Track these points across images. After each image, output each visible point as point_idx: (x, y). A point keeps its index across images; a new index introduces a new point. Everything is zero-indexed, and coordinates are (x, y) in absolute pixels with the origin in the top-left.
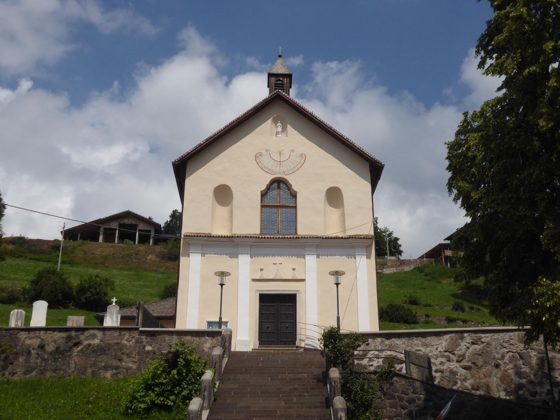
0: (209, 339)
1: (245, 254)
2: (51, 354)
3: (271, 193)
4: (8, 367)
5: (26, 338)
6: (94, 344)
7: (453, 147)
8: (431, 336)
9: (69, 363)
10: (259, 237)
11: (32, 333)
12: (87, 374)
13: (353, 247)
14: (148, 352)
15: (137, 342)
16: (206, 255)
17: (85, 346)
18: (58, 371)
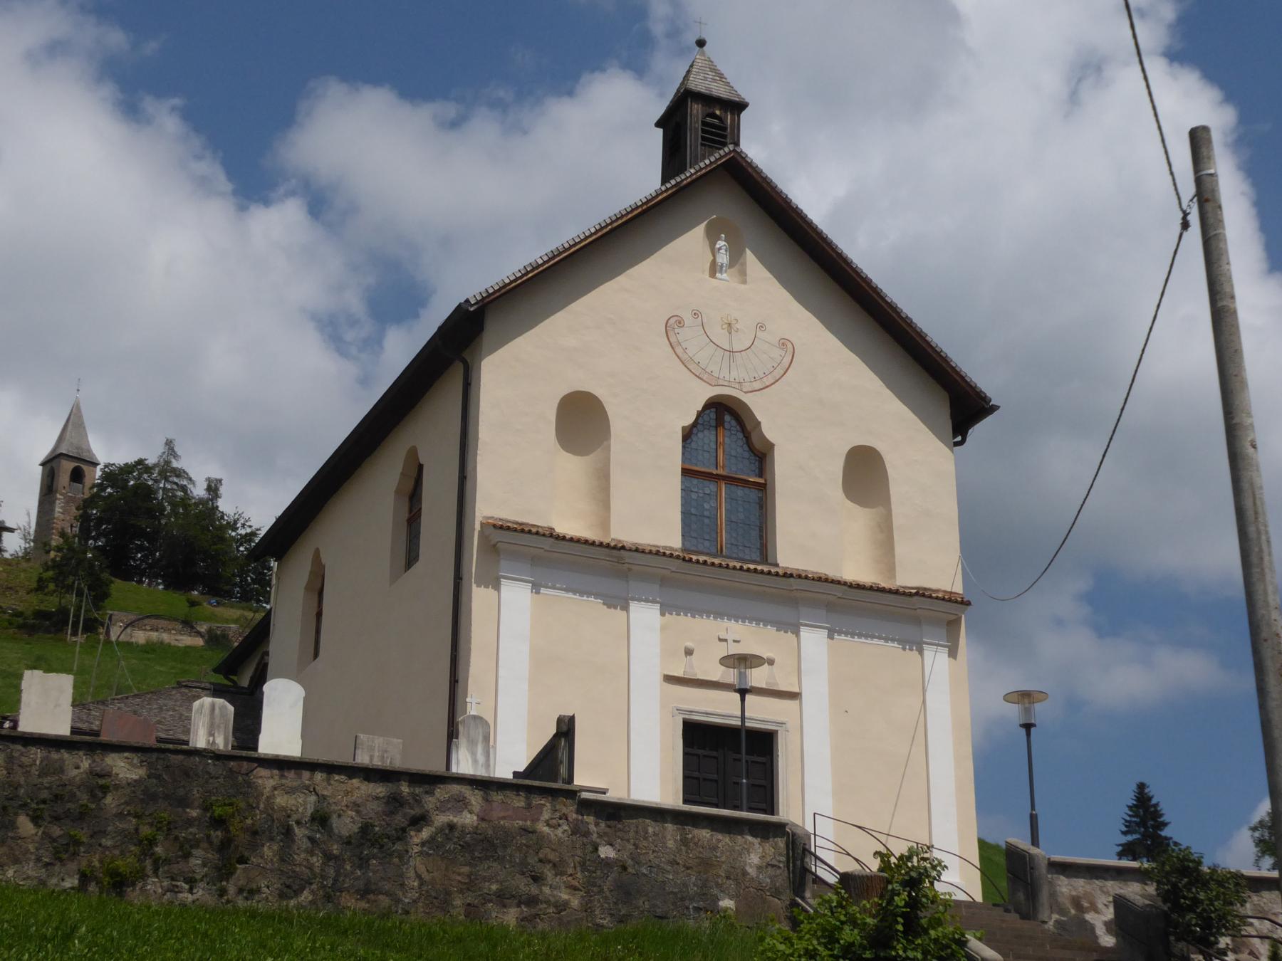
0: (756, 841)
1: (647, 601)
2: (349, 843)
3: (700, 435)
4: (236, 869)
5: (275, 788)
6: (463, 826)
7: (460, 305)
8: (1270, 889)
9: (402, 876)
10: (678, 557)
11: (291, 774)
12: (454, 912)
13: (917, 621)
14: (607, 863)
15: (575, 832)
16: (543, 590)
17: (440, 830)
18: (371, 897)
